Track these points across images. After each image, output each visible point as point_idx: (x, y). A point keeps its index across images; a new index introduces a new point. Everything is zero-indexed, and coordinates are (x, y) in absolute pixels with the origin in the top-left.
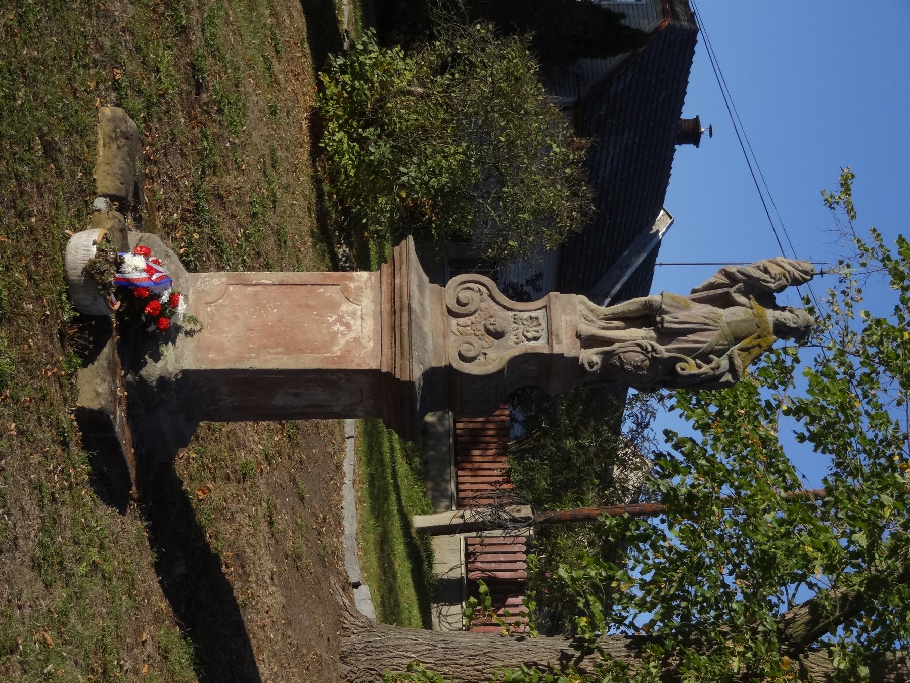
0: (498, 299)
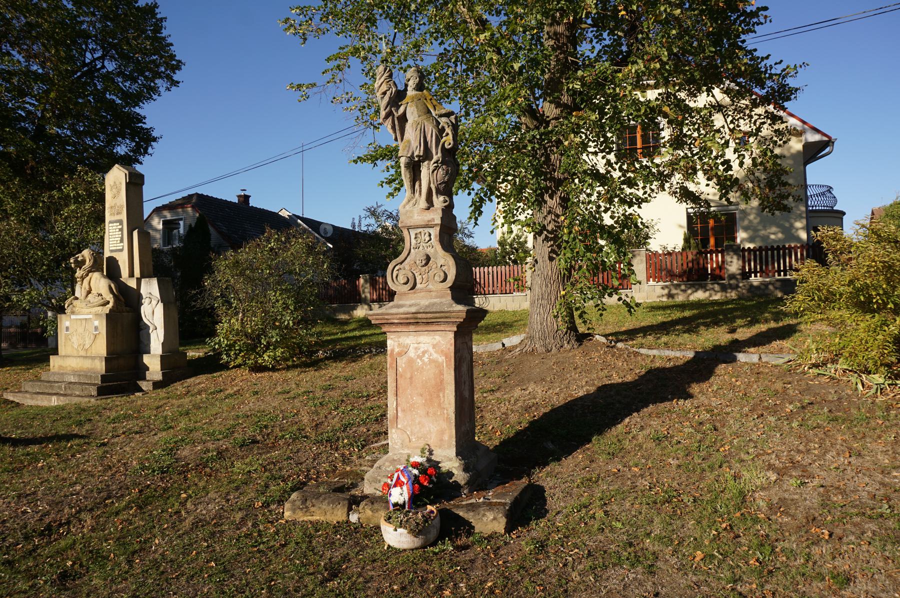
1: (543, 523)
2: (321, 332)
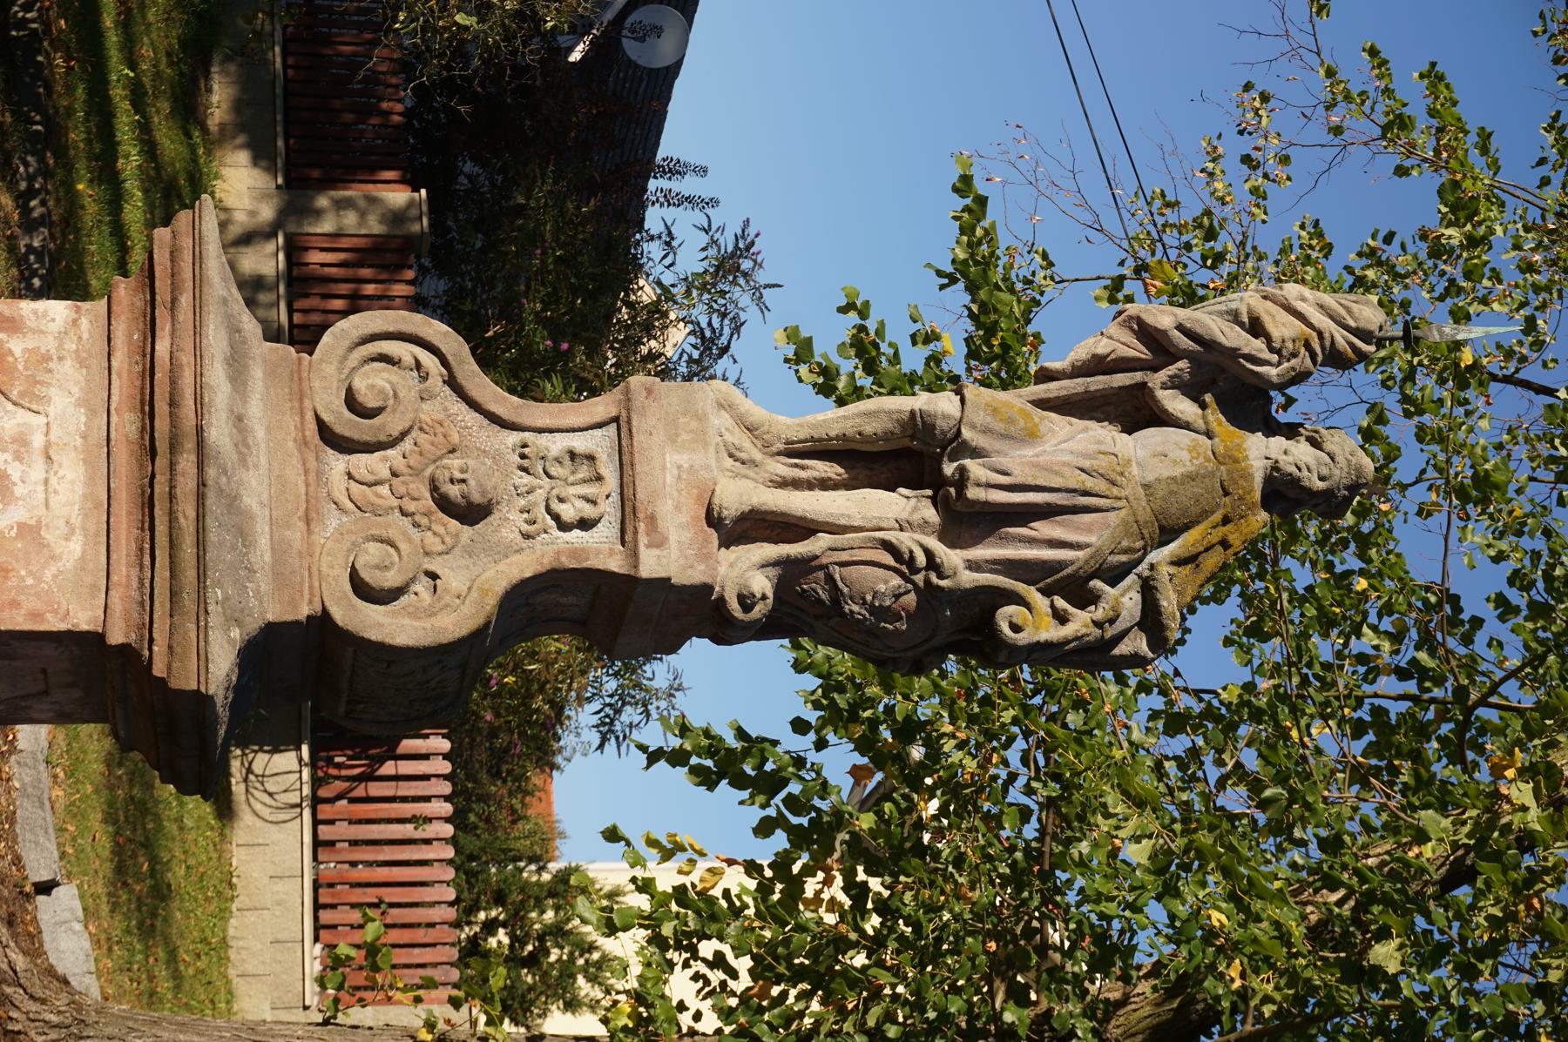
0: (474, 393)
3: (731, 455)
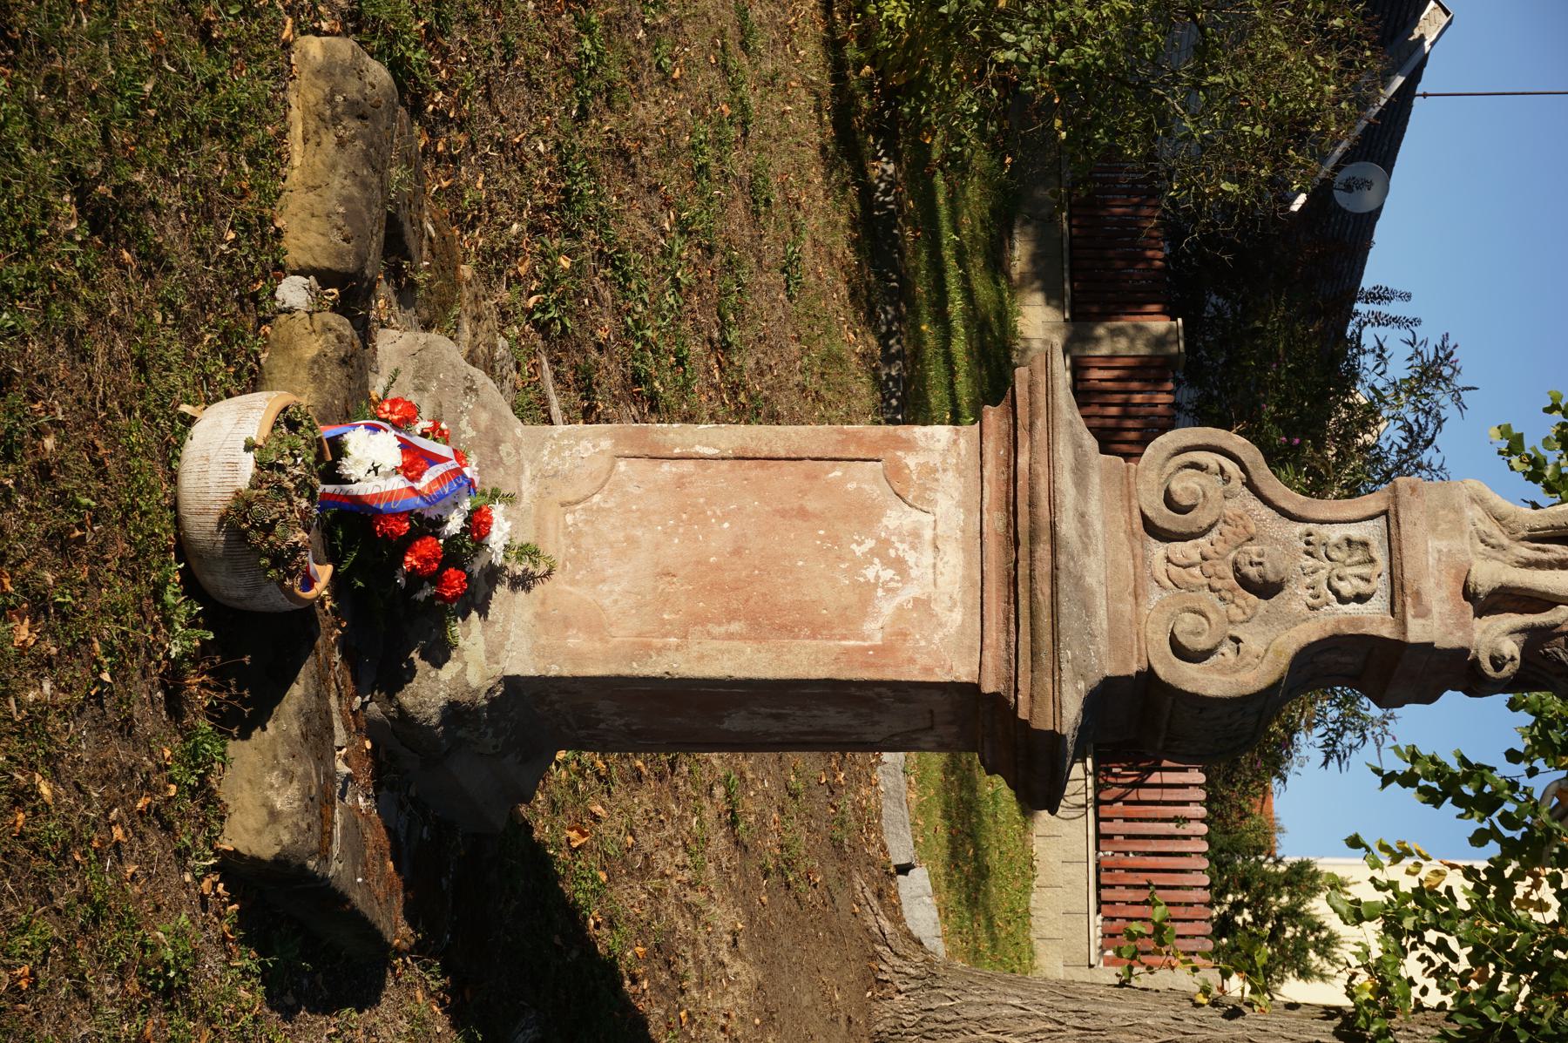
0: (1268, 492)
1: (250, 996)
2: (964, 170)
3: (1483, 541)
